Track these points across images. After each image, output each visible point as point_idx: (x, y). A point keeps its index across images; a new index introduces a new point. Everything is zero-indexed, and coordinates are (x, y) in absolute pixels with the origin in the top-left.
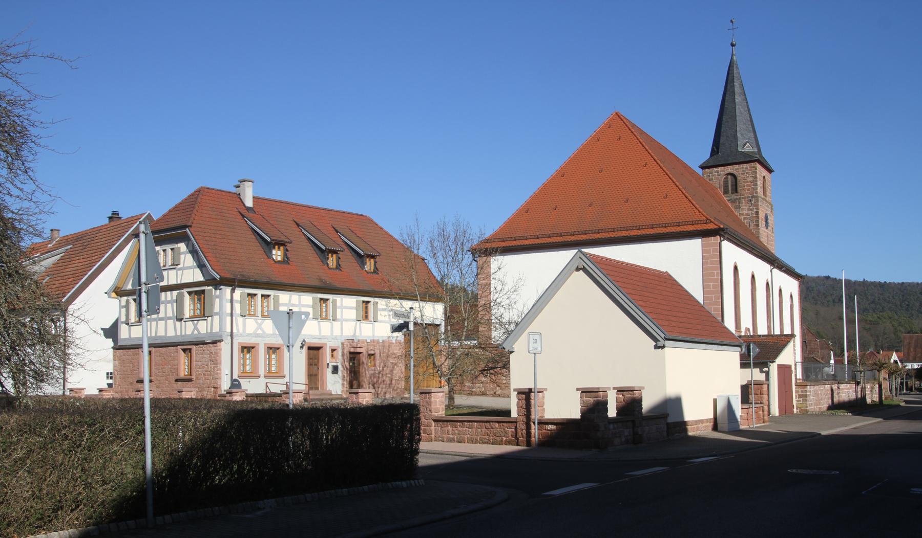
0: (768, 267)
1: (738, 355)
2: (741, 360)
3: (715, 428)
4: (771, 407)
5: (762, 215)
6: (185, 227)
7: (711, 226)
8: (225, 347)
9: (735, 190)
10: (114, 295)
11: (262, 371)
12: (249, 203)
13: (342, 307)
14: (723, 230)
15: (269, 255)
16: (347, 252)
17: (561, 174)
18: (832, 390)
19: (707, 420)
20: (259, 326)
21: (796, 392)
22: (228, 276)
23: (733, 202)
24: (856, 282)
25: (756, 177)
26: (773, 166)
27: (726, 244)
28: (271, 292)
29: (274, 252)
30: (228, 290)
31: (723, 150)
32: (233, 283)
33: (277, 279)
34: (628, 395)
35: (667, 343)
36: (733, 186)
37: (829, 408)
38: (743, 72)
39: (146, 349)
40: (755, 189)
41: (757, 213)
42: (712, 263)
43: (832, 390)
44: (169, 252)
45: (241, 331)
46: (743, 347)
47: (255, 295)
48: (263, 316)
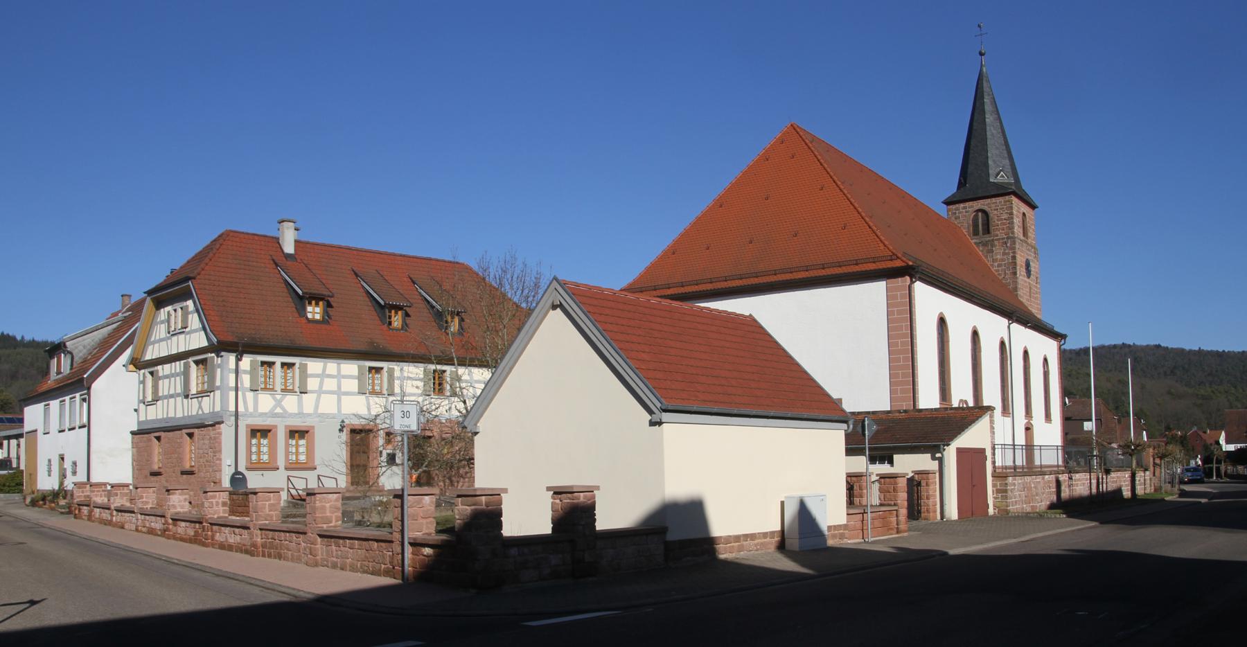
0: (1005, 321)
1: (843, 433)
2: (847, 443)
3: (782, 546)
4: (946, 508)
5: (1020, 261)
6: (187, 279)
7: (898, 264)
8: (226, 431)
9: (987, 230)
10: (131, 367)
11: (281, 462)
12: (289, 248)
13: (402, 379)
14: (912, 268)
15: (302, 311)
16: (423, 305)
17: (720, 203)
18: (1058, 483)
19: (773, 533)
20: (278, 403)
21: (994, 485)
22: (230, 338)
23: (985, 244)
24: (1190, 351)
25: (1011, 214)
26: (1037, 202)
27: (919, 287)
28: (296, 360)
29: (309, 309)
30: (232, 358)
31: (973, 182)
32: (240, 349)
33: (305, 342)
34: (567, 500)
35: (666, 416)
36: (984, 225)
37: (1052, 507)
38: (996, 87)
39: (281, 435)
40: (1011, 228)
41: (1014, 258)
42: (899, 312)
43: (1058, 483)
44: (179, 311)
45: (251, 409)
46: (851, 423)
47: (274, 363)
48: (283, 390)
